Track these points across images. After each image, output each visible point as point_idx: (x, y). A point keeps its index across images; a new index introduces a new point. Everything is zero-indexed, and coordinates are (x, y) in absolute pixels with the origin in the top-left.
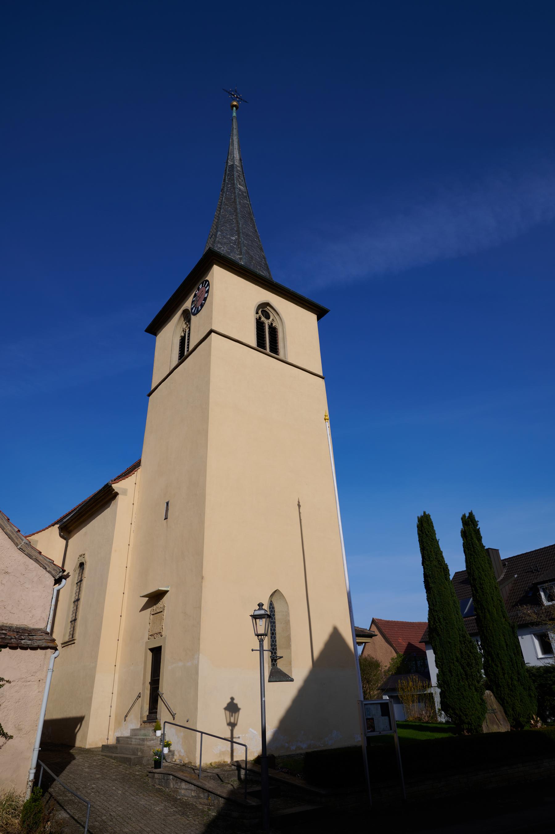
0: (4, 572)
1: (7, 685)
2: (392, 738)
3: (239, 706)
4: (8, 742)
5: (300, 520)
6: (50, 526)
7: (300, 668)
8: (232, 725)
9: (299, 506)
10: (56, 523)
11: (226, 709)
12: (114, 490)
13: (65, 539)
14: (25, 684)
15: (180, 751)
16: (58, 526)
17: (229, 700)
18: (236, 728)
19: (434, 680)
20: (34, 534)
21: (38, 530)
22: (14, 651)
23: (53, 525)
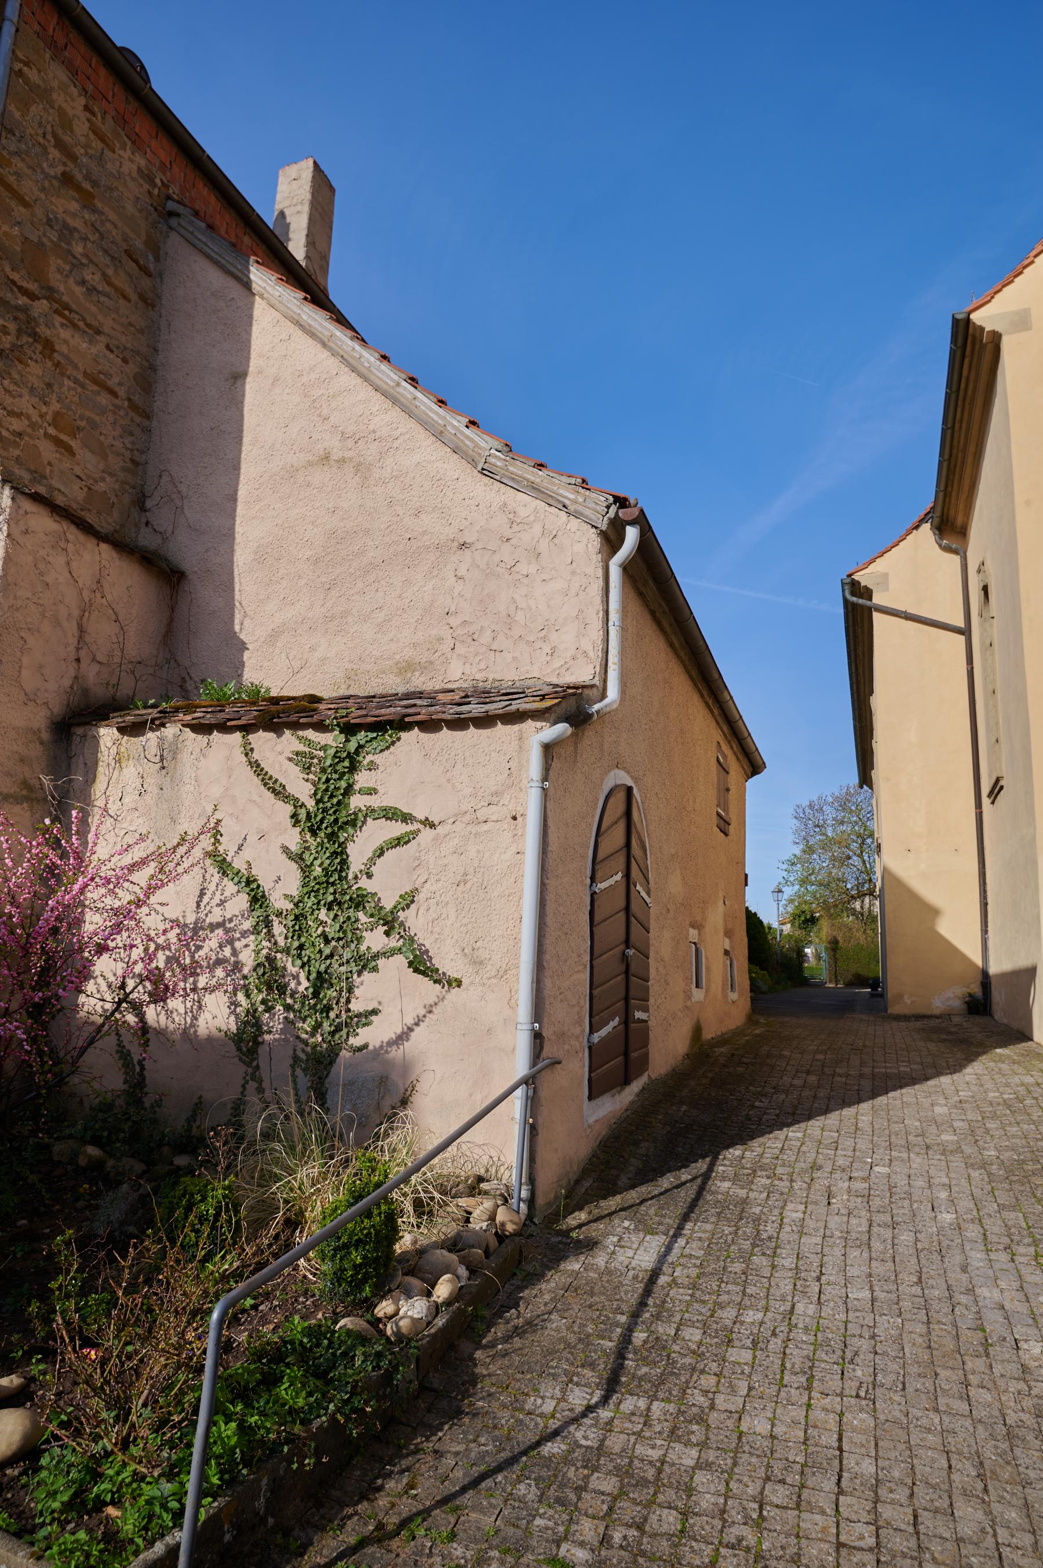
0: (456, 544)
1: (427, 833)
4: (449, 996)
6: (909, 533)
10: (922, 521)
12: (982, 329)
13: (955, 552)
14: (474, 829)
16: (928, 525)
20: (873, 561)
21: (883, 549)
22: (432, 735)
23: (917, 527)
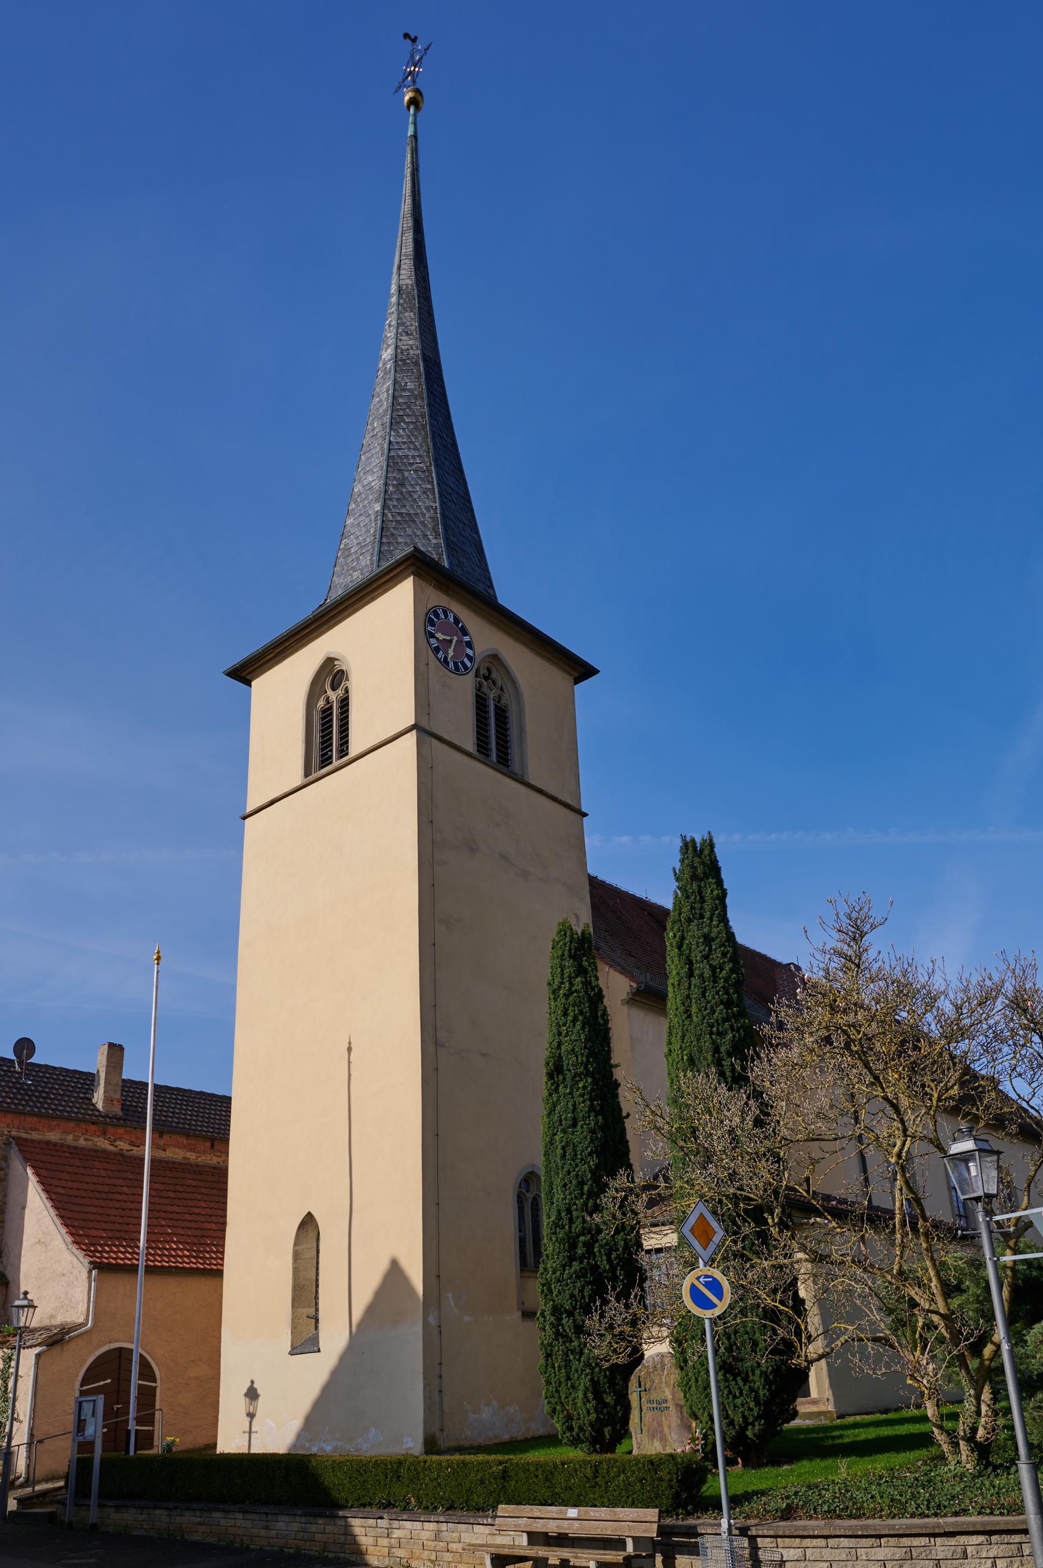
2: (745, 1465)
3: (259, 1392)
5: (349, 1075)
7: (334, 1337)
8: (251, 1416)
9: (349, 1049)
11: (246, 1395)
15: (565, 994)
17: (249, 1384)
18: (255, 1420)
19: (487, 1457)
